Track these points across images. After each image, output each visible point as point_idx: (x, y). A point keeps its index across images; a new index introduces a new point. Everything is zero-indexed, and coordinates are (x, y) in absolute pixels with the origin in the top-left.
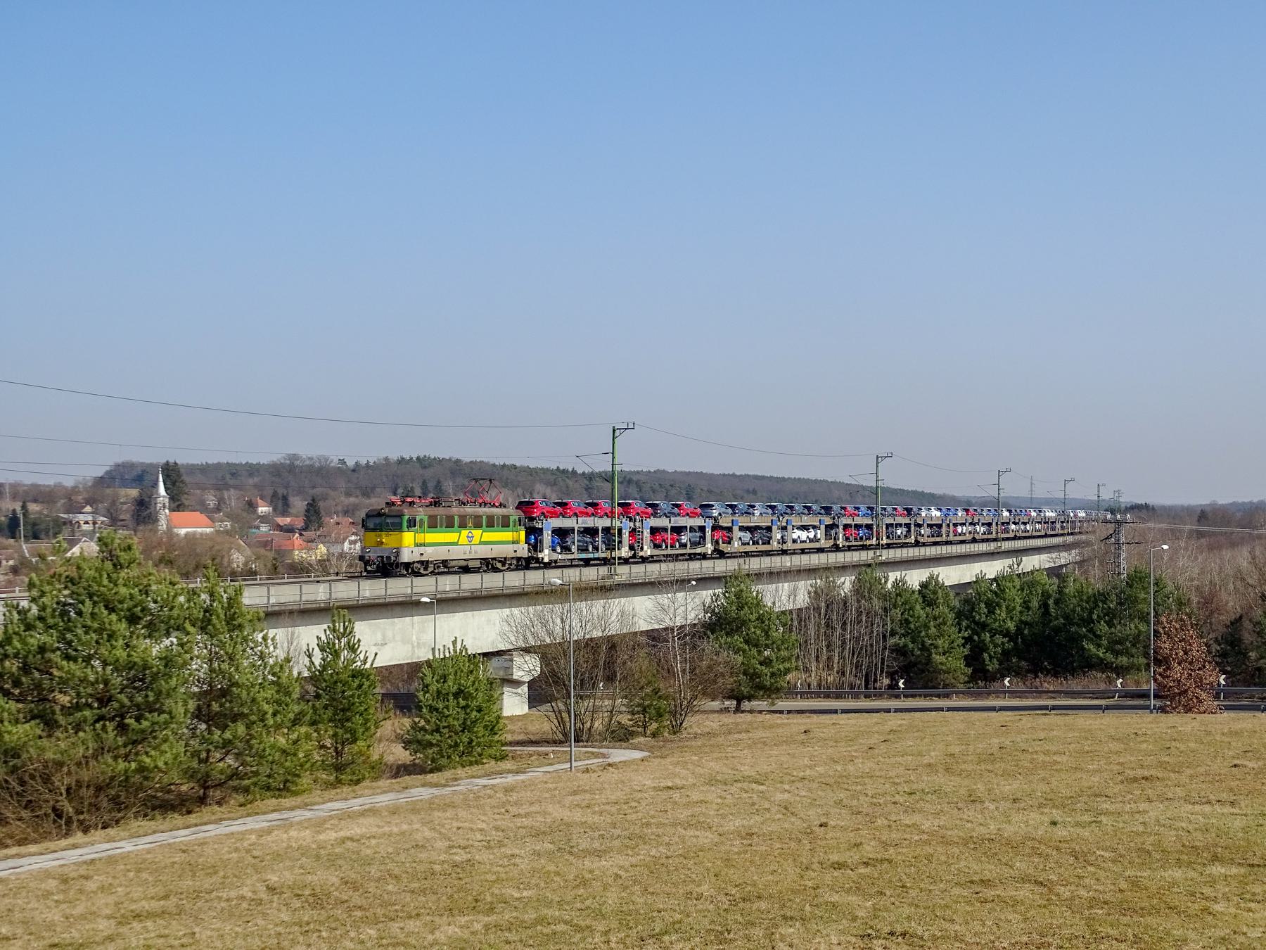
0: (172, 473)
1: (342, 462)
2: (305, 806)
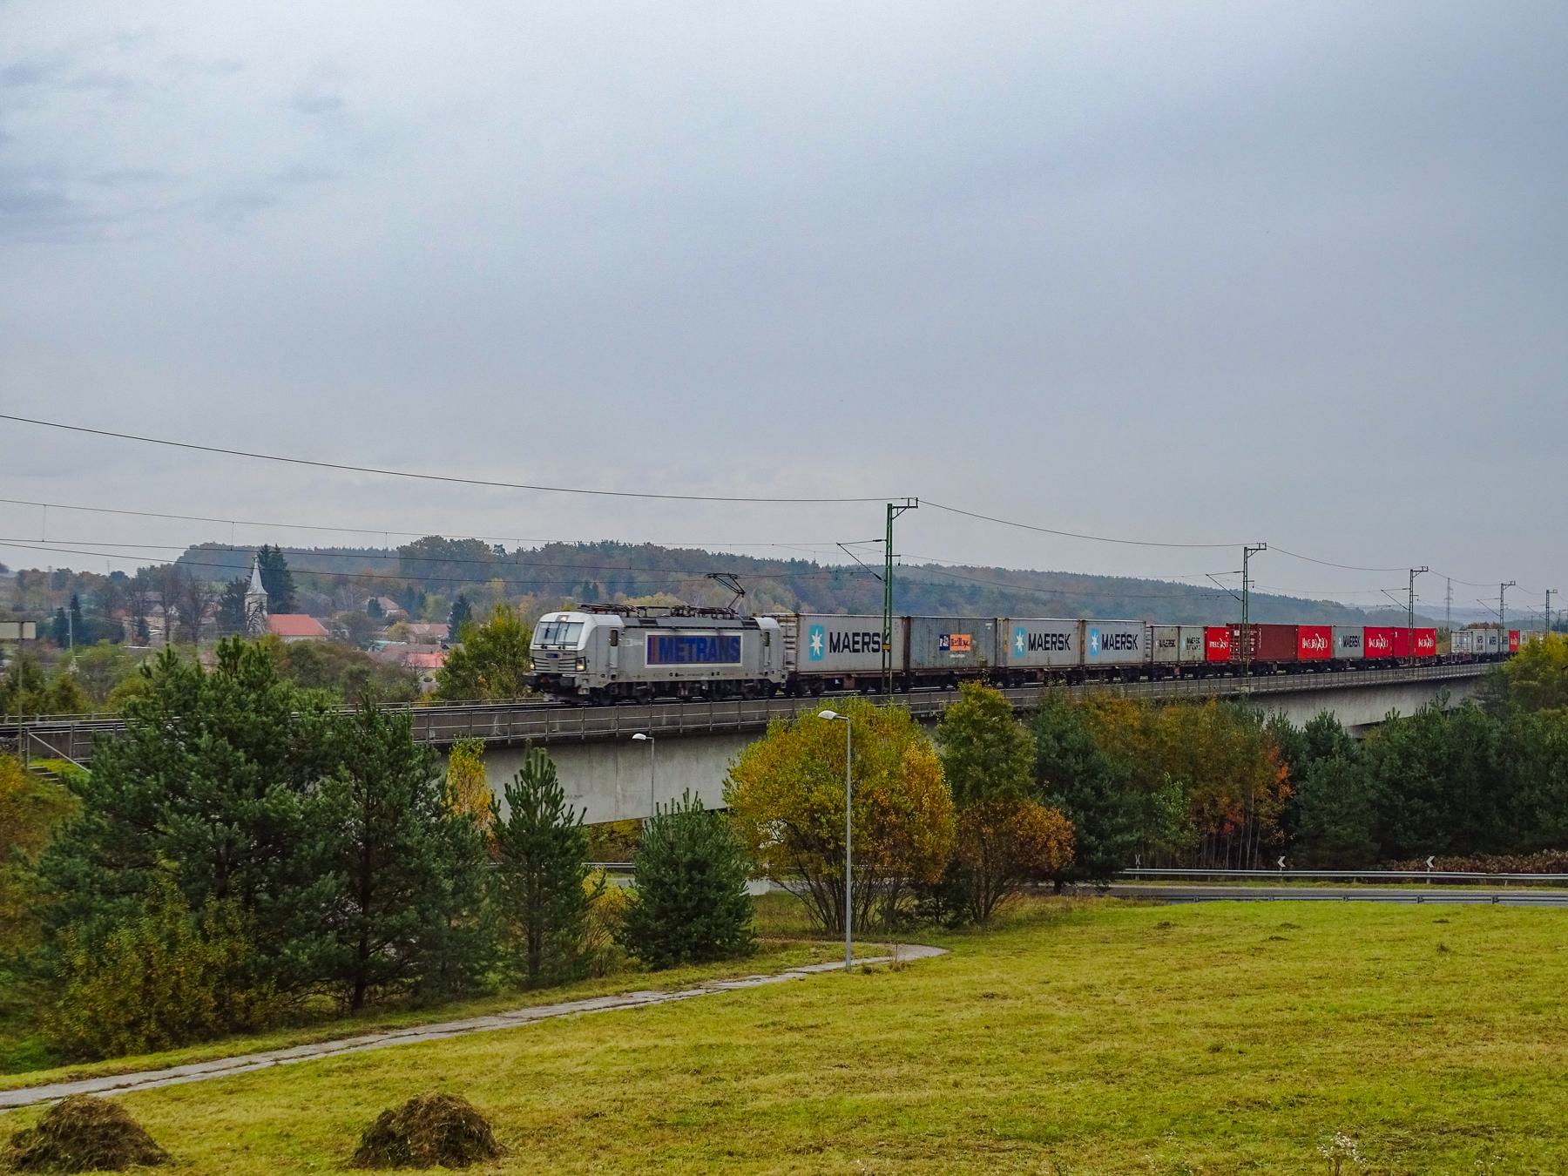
0: (272, 562)
1: (500, 548)
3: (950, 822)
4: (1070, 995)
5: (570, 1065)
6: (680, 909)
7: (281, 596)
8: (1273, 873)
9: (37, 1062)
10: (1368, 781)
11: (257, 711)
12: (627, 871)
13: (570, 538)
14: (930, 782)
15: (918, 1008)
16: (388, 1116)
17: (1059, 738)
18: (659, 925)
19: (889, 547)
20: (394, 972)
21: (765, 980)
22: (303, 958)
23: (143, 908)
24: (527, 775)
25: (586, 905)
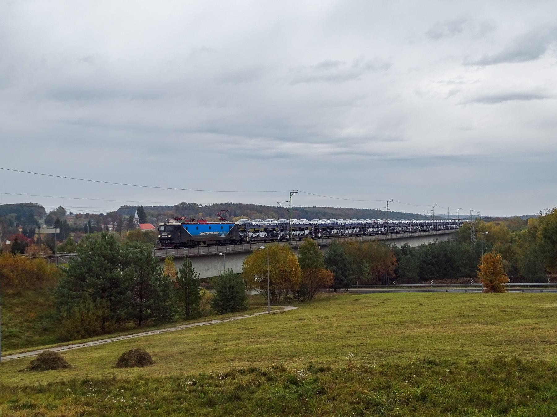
0: (140, 210)
2: (174, 327)
3: (300, 274)
4: (320, 319)
5: (186, 340)
6: (227, 299)
7: (143, 219)
8: (392, 285)
9: (54, 342)
10: (416, 261)
11: (110, 250)
12: (212, 289)
13: (219, 202)
14: (295, 264)
15: (280, 323)
16: (124, 354)
17: (334, 252)
18: (222, 303)
19: (290, 203)
20: (150, 316)
21: (248, 316)
22: (123, 313)
23: (81, 301)
24: (184, 265)
25: (200, 298)
